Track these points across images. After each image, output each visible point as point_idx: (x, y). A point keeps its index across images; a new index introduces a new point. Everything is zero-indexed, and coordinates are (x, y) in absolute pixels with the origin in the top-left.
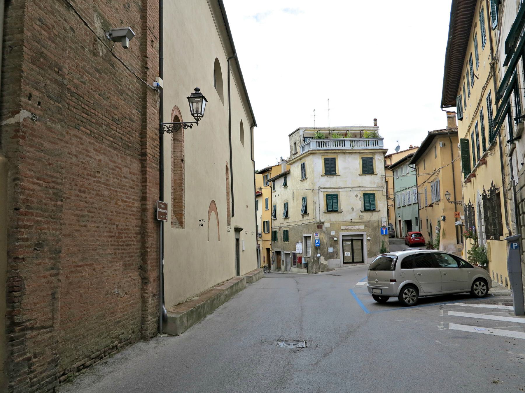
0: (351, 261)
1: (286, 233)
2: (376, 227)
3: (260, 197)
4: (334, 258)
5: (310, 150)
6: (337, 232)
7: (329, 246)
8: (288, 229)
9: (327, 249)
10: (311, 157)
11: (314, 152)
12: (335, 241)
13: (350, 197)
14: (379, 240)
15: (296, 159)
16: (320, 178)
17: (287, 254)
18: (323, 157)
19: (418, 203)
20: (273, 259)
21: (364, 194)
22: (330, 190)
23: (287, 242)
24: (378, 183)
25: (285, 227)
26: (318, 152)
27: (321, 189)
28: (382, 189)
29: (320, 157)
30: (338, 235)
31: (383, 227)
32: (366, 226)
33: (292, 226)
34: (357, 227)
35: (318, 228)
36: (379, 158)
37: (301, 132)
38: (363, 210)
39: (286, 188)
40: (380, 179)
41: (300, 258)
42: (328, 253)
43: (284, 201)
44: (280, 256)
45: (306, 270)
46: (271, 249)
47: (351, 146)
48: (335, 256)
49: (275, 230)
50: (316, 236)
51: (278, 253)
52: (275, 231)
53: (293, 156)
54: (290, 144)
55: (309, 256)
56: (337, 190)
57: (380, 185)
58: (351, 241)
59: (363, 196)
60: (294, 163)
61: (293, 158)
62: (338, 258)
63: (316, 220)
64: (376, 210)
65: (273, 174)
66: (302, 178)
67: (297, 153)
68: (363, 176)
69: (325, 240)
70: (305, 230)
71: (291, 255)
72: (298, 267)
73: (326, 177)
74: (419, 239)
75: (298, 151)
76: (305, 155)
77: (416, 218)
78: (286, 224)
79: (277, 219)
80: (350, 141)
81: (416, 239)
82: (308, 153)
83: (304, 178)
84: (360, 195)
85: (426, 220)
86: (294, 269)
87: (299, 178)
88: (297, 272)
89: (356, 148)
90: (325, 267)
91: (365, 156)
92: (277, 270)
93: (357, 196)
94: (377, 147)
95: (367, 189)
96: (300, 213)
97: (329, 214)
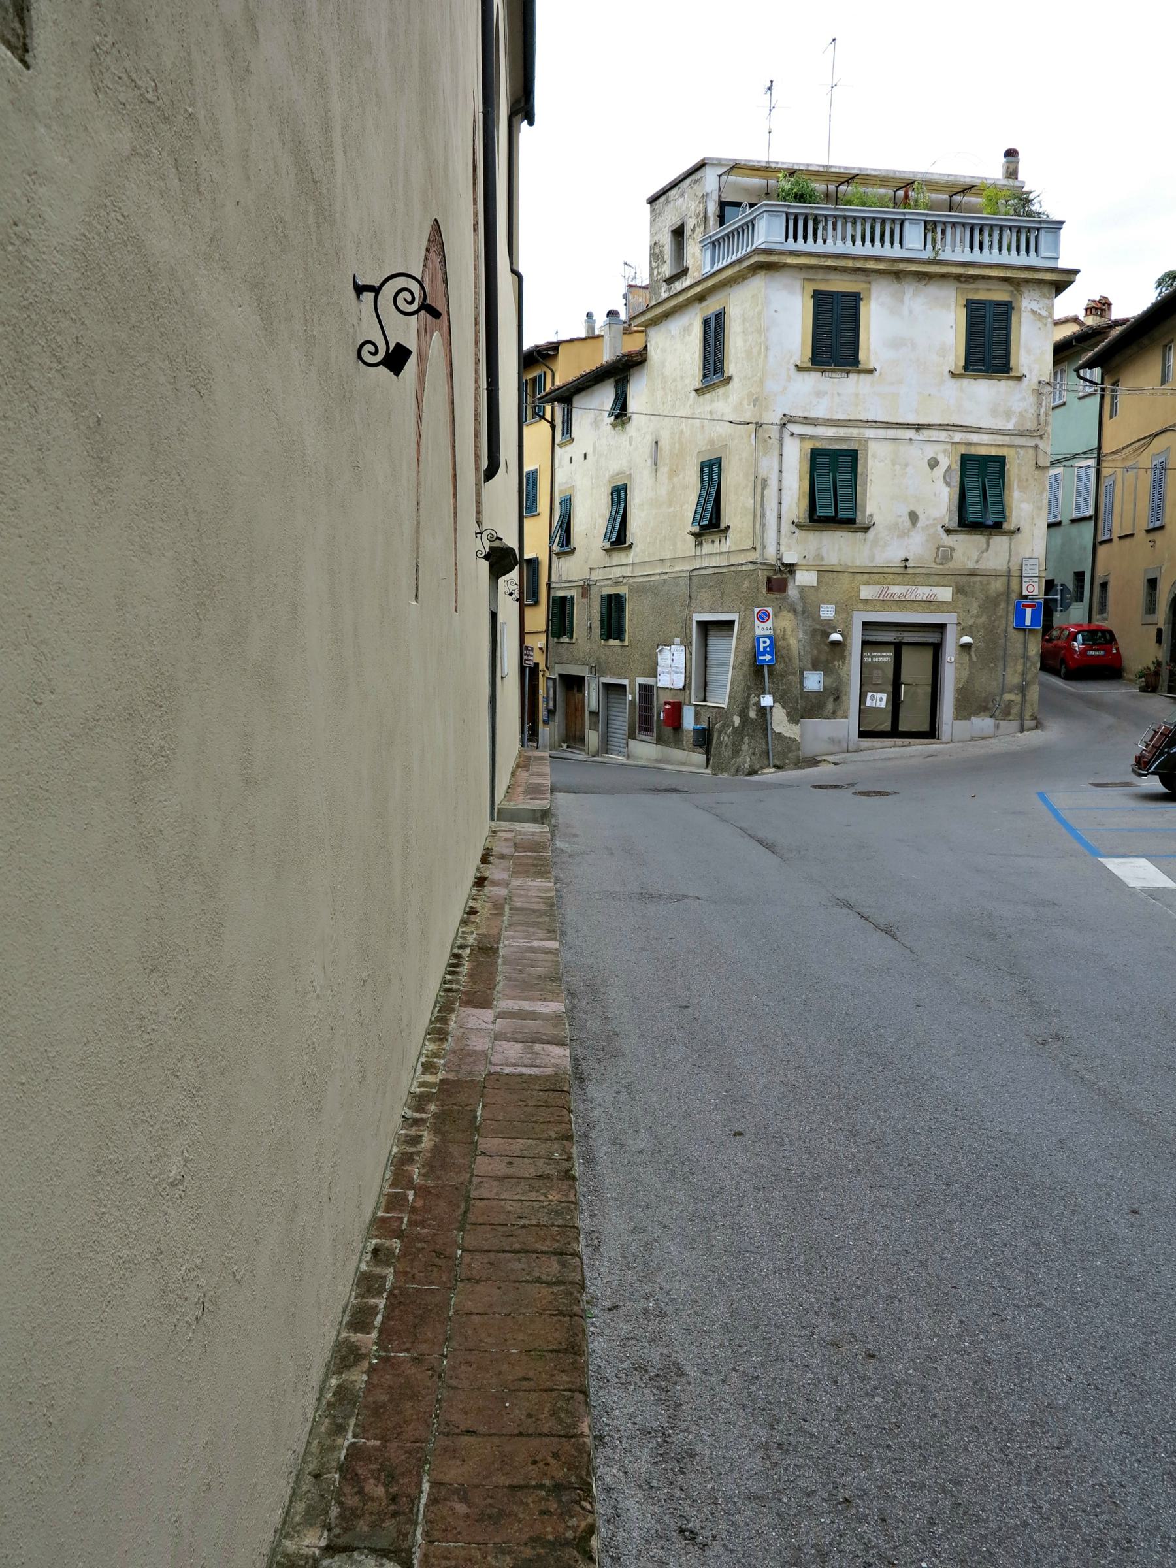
0: (889, 729)
1: (613, 608)
2: (999, 595)
3: (639, 367)
4: (825, 714)
5: (757, 251)
6: (844, 609)
7: (810, 666)
8: (622, 590)
9: (802, 674)
10: (758, 283)
11: (774, 259)
12: (836, 644)
13: (907, 465)
14: (1005, 650)
15: (681, 298)
16: (789, 379)
17: (613, 690)
18: (806, 284)
19: (1095, 518)
20: (551, 704)
21: (965, 459)
22: (830, 432)
23: (617, 642)
24: (1021, 414)
25: (609, 582)
26: (790, 260)
27: (793, 428)
28: (1037, 441)
29: (798, 284)
30: (848, 622)
31: (1026, 597)
32: (959, 590)
33: (641, 580)
34: (923, 592)
35: (769, 590)
36: (1035, 306)
37: (710, 180)
38: (954, 524)
39: (624, 424)
40: (1032, 399)
41: (676, 710)
42: (807, 695)
43: (612, 477)
44: (578, 696)
45: (699, 757)
46: (542, 666)
47: (929, 246)
48: (830, 706)
49: (561, 593)
50: (762, 620)
51: (574, 684)
52: (563, 599)
53: (664, 287)
54: (652, 235)
55: (720, 699)
56: (854, 432)
57: (1030, 425)
58: (892, 648)
59: (956, 467)
60: (667, 315)
61: (664, 295)
62: (839, 713)
63: (762, 554)
64: (1005, 526)
65: (563, 373)
66: (704, 376)
67: (684, 272)
68: (965, 382)
69: (796, 641)
70: (704, 595)
71: (633, 694)
72: (660, 741)
73: (815, 376)
74: (1102, 653)
75: (689, 262)
76: (729, 272)
77: (1079, 576)
78: (618, 572)
79: (573, 551)
80: (926, 222)
81: (1091, 653)
82: (746, 264)
83: (716, 379)
84: (949, 461)
85: (1141, 587)
86: (645, 750)
87: (687, 381)
88: (657, 761)
89: (946, 255)
90: (790, 751)
91: (982, 296)
92: (565, 746)
93: (933, 464)
94: (1032, 260)
95: (975, 438)
96: (688, 525)
97: (817, 533)
